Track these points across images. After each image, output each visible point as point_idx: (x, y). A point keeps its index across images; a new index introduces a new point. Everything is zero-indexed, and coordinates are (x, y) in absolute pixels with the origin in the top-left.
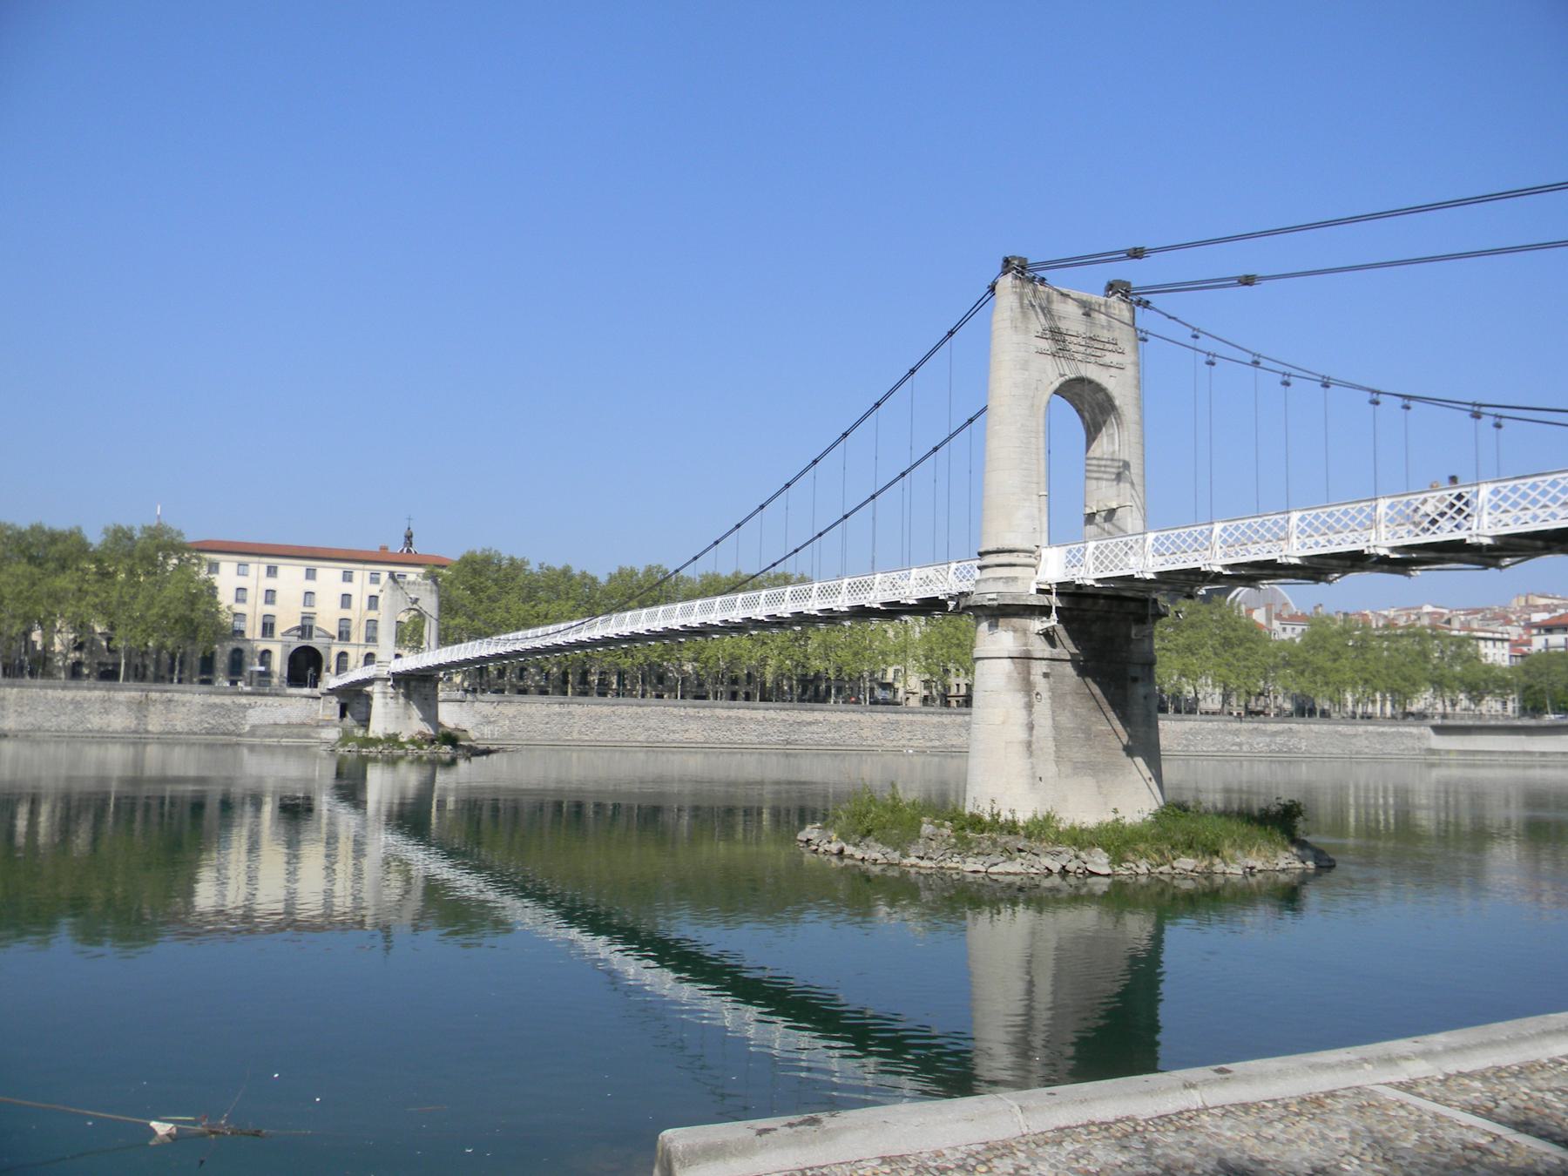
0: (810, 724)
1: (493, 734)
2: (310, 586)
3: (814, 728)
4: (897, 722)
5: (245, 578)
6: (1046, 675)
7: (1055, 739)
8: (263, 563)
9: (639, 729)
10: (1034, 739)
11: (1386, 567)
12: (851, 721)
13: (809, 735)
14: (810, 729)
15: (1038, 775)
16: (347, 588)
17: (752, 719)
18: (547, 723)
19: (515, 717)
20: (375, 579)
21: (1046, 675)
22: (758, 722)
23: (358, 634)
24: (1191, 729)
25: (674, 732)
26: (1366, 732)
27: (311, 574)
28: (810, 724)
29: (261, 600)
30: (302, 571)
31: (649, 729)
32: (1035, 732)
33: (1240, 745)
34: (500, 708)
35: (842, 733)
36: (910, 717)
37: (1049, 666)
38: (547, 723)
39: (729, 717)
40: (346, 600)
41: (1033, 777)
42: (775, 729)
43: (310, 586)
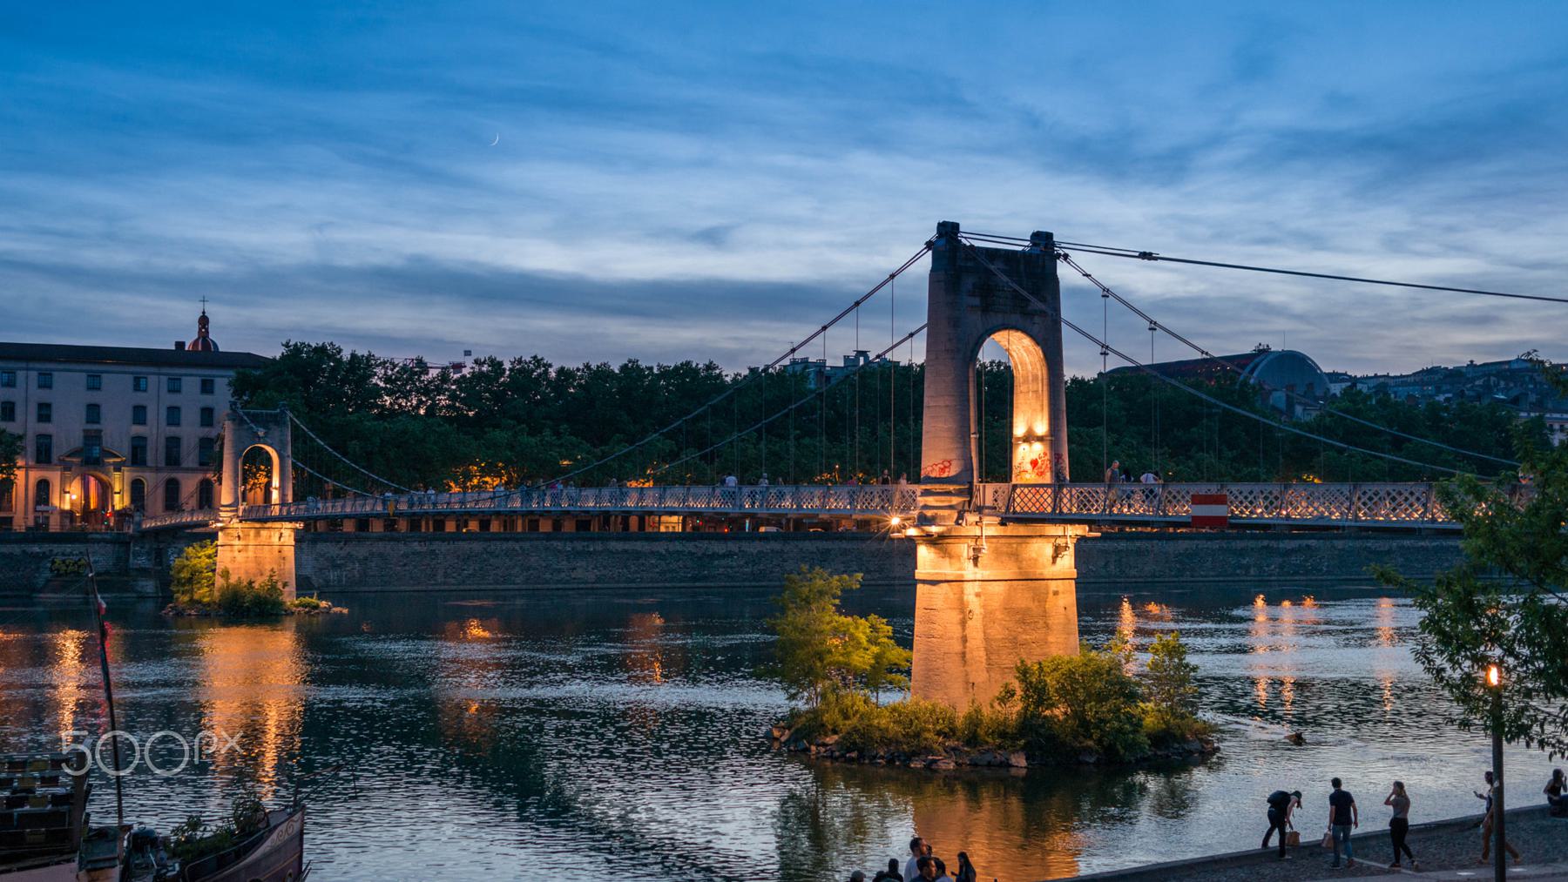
0: (725, 556)
1: (340, 581)
2: (95, 397)
3: (728, 561)
4: (828, 551)
5: (47, 391)
6: (978, 595)
7: (986, 649)
8: (33, 369)
9: (517, 569)
10: (967, 650)
11: (100, 491)
12: (772, 551)
13: (721, 570)
14: (723, 562)
15: (971, 681)
16: (139, 399)
17: (653, 553)
18: (405, 565)
19: (366, 559)
20: (207, 387)
21: (978, 595)
22: (661, 557)
23: (190, 456)
24: (1187, 549)
25: (559, 571)
26: (1402, 547)
27: (94, 384)
28: (725, 556)
29: (33, 417)
30: (129, 379)
31: (528, 569)
32: (968, 644)
33: (1247, 568)
34: (348, 549)
35: (762, 567)
36: (844, 545)
37: (980, 586)
38: (405, 565)
39: (626, 551)
40: (139, 414)
41: (967, 683)
42: (681, 564)
43: (95, 397)
